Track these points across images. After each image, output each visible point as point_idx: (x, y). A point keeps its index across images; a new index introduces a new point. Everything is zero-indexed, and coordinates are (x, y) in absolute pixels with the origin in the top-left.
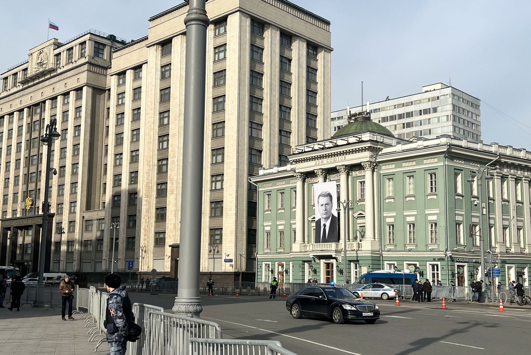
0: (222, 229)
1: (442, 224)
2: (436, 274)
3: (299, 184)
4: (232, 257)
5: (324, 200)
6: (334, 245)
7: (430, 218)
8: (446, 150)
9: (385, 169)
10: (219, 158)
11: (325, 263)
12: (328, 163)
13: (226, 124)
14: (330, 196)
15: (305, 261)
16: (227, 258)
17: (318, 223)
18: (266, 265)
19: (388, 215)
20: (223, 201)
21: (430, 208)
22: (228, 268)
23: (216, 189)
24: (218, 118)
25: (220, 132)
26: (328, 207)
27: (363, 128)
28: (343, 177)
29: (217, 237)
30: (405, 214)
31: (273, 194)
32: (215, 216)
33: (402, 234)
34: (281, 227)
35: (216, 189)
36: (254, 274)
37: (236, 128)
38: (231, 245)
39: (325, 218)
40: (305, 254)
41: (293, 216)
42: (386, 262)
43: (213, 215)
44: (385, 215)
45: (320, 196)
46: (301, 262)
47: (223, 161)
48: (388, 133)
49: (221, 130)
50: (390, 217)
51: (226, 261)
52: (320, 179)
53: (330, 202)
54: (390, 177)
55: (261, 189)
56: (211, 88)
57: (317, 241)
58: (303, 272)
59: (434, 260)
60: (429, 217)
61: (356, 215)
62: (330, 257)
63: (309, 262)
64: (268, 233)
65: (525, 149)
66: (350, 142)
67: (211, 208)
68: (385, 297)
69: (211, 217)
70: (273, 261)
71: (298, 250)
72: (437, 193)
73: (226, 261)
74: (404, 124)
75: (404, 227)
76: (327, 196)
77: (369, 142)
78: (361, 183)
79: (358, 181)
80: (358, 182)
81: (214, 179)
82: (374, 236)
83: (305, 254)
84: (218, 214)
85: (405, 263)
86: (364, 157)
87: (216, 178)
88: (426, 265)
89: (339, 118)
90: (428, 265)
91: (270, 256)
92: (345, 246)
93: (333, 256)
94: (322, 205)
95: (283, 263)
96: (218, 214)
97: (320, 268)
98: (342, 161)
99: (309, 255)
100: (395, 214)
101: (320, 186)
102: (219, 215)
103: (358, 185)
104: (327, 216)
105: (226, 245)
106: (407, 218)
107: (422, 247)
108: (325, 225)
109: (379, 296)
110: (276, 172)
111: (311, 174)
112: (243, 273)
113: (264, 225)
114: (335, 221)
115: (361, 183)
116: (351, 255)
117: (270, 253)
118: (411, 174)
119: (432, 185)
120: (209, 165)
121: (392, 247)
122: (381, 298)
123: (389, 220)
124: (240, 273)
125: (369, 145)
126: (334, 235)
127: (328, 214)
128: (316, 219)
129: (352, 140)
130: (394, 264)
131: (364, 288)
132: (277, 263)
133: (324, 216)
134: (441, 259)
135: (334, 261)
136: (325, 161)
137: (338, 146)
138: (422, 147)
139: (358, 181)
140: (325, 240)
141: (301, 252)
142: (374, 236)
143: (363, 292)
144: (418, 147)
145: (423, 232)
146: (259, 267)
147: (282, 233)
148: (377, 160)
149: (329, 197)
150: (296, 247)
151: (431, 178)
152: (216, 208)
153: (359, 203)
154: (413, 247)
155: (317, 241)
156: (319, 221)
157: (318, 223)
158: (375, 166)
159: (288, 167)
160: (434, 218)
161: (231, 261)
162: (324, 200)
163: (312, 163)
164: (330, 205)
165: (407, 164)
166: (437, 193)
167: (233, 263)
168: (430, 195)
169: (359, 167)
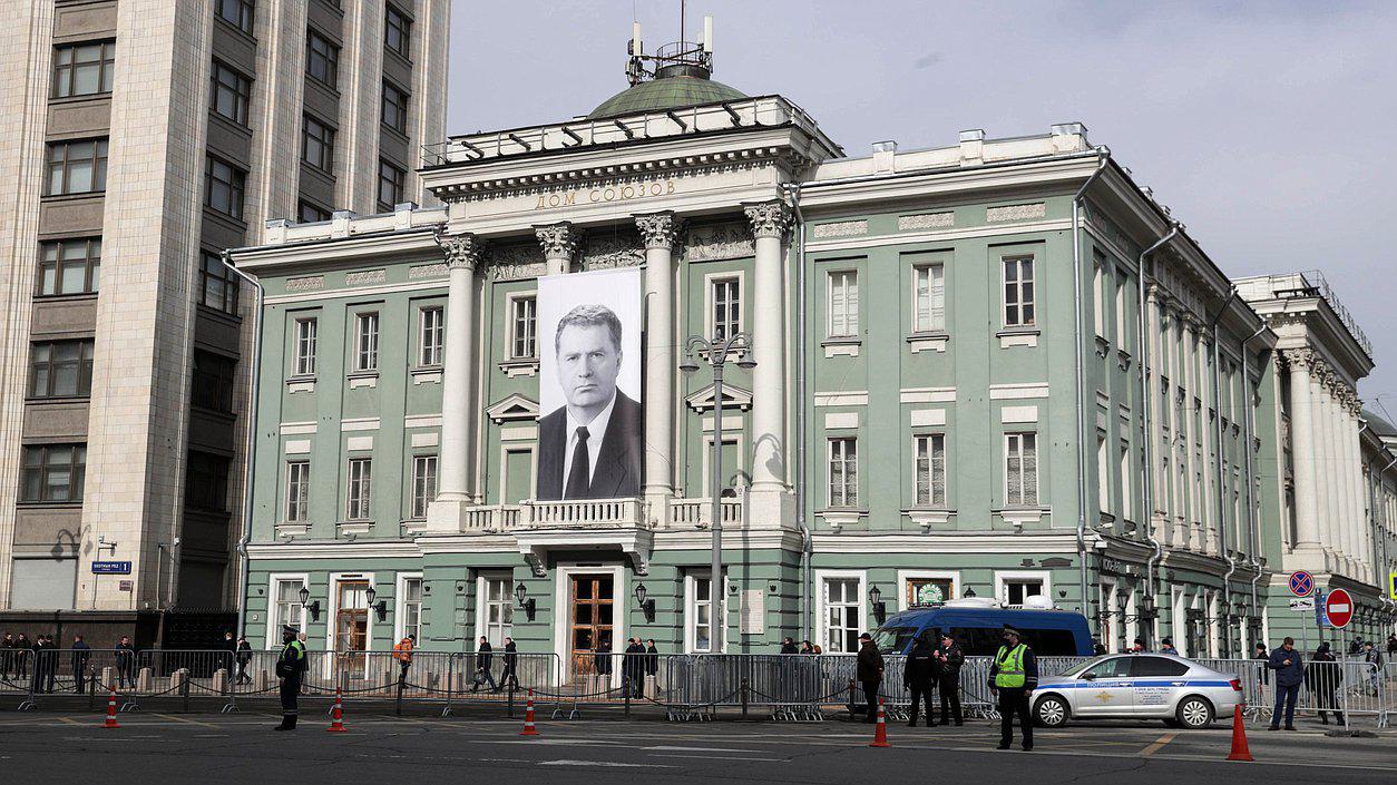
0: (84, 445)
3: (458, 279)
4: (130, 552)
5: (582, 339)
6: (629, 504)
7: (1011, 415)
8: (1091, 173)
9: (821, 238)
10: (81, 179)
11: (574, 577)
13: (120, 51)
14: (612, 323)
15: (475, 571)
16: (106, 557)
17: (554, 428)
19: (832, 402)
20: (92, 340)
21: (921, 382)
22: (114, 596)
23: (59, 295)
24: (81, 23)
25: (87, 81)
26: (600, 365)
28: (658, 255)
29: (57, 479)
30: (905, 398)
32: (51, 397)
33: (886, 470)
34: (297, 447)
35: (59, 295)
36: (231, 620)
37: (166, 66)
38: (118, 504)
39: (585, 407)
40: (487, 544)
43: (42, 391)
44: (818, 402)
45: (565, 321)
46: (463, 574)
47: (97, 192)
49: (94, 72)
50: (839, 412)
51: (98, 569)
52: (557, 261)
53: (609, 346)
54: (844, 268)
57: (549, 486)
58: (471, 610)
60: (1005, 410)
61: (498, 412)
62: (613, 554)
63: (499, 575)
64: (300, 467)
67: (35, 368)
68: (1196, 713)
69: (31, 399)
70: (320, 569)
71: (454, 527)
72: (377, 370)
73: (98, 569)
75: (993, 448)
76: (597, 322)
77: (788, 132)
78: (520, 302)
79: (708, 277)
80: (708, 283)
81: (52, 255)
82: (672, 480)
83: (487, 544)
84: (66, 386)
85: (903, 575)
86: (756, 186)
87: (62, 254)
88: (895, 583)
91: (307, 552)
92: (661, 511)
94: (575, 357)
95: (365, 576)
96: (66, 386)
97: (550, 595)
98: (656, 197)
99: (514, 544)
100: (376, 426)
101: (560, 289)
102: (73, 391)
103: (509, 313)
104: (594, 397)
105: (104, 509)
106: (1005, 410)
107: (883, 517)
108: (584, 434)
109: (1168, 709)
110: (407, 227)
111: (524, 246)
112: (167, 614)
114: (628, 421)
115: (520, 302)
116: (698, 547)
117: (306, 541)
118: (928, 261)
119: (365, 347)
120: (36, 199)
121: (299, 532)
122: (1176, 722)
123: (835, 421)
124: (157, 615)
126: (620, 468)
127: (599, 391)
128: (545, 410)
129: (660, 126)
130: (299, 583)
131: (1090, 677)
132: (334, 577)
133: (584, 399)
134: (1052, 563)
135: (619, 573)
136: (583, 195)
137: (482, 160)
138: (979, 163)
139: (510, 295)
140: (580, 488)
141: (462, 534)
142: (672, 480)
143: (1091, 691)
144: (964, 164)
145: (978, 464)
146: (253, 591)
147: (361, 464)
148: (802, 203)
149: (605, 328)
150: (444, 516)
151: (365, 328)
152: (54, 367)
153: (512, 372)
154: (363, 530)
155: (549, 486)
156: (560, 417)
157: (554, 428)
158: (791, 221)
160: (1029, 414)
161: (123, 568)
162: (582, 339)
163: (729, 179)
164: (612, 356)
165: (919, 221)
166: (377, 370)
167: (134, 577)
168: (356, 377)
169: (732, 224)
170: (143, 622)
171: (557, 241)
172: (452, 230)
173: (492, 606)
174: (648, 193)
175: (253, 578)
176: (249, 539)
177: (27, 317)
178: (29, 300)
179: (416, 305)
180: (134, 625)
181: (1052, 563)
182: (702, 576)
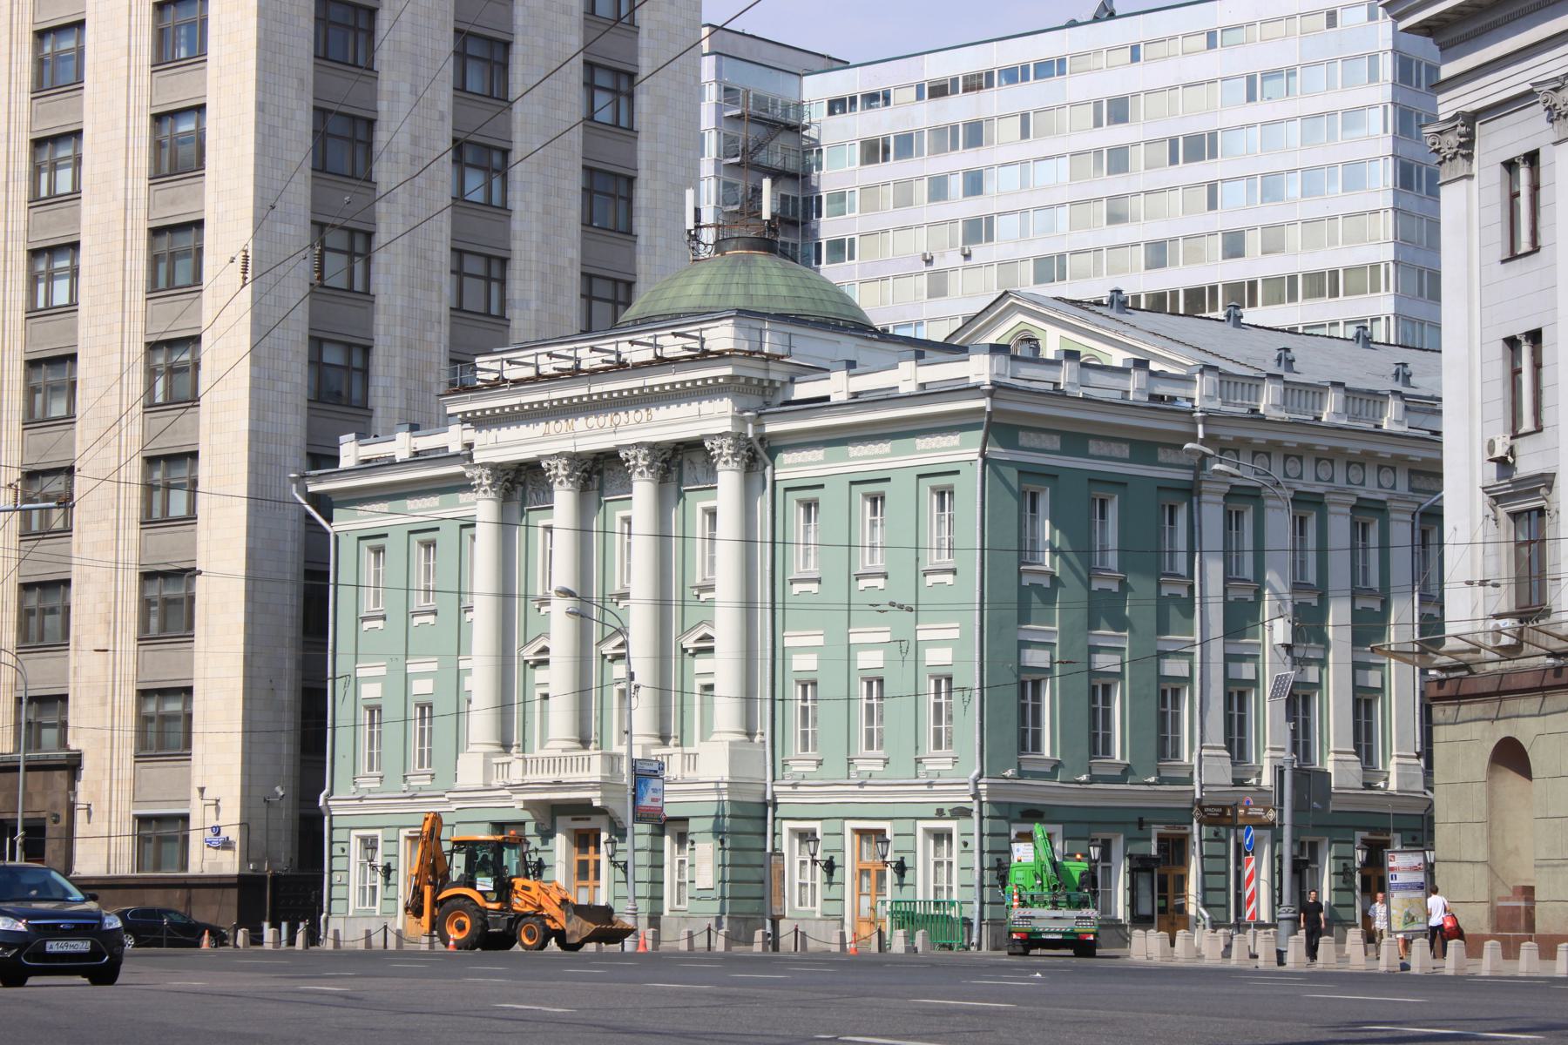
1: (969, 676)
2: (592, 865)
3: (483, 507)
10: (58, 408)
12: (591, 434)
18: (364, 839)
24: (173, 202)
27: (734, 290)
31: (395, 545)
41: (461, 646)
42: (787, 825)
48: (830, 310)
55: (344, 524)
56: (147, 70)
59: (940, 814)
61: (690, 643)
65: (1341, 385)
66: (668, 353)
71: (478, 782)
74: (1173, 142)
86: (712, 419)
88: (397, 841)
89: (871, 98)
90: (848, 833)
93: (597, 803)
112: (276, 878)
113: (363, 675)
125: (728, 371)
129: (672, 346)
132: (404, 832)
134: (961, 813)
146: (337, 849)
150: (470, 772)
158: (756, 455)
159: (453, 438)
170: (246, 886)
171: (725, 451)
172: (479, 458)
173: (580, 862)
174: (632, 421)
175: (337, 835)
176: (332, 793)
177: (134, 545)
178: (136, 525)
179: (858, 491)
180: (233, 894)
181: (961, 813)
182: (680, 828)
